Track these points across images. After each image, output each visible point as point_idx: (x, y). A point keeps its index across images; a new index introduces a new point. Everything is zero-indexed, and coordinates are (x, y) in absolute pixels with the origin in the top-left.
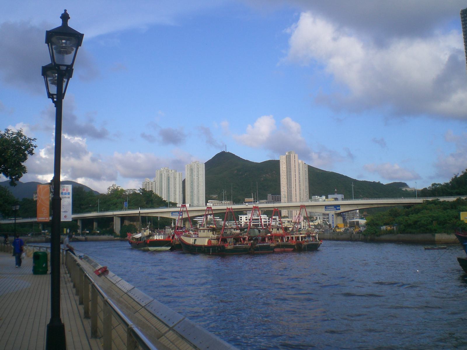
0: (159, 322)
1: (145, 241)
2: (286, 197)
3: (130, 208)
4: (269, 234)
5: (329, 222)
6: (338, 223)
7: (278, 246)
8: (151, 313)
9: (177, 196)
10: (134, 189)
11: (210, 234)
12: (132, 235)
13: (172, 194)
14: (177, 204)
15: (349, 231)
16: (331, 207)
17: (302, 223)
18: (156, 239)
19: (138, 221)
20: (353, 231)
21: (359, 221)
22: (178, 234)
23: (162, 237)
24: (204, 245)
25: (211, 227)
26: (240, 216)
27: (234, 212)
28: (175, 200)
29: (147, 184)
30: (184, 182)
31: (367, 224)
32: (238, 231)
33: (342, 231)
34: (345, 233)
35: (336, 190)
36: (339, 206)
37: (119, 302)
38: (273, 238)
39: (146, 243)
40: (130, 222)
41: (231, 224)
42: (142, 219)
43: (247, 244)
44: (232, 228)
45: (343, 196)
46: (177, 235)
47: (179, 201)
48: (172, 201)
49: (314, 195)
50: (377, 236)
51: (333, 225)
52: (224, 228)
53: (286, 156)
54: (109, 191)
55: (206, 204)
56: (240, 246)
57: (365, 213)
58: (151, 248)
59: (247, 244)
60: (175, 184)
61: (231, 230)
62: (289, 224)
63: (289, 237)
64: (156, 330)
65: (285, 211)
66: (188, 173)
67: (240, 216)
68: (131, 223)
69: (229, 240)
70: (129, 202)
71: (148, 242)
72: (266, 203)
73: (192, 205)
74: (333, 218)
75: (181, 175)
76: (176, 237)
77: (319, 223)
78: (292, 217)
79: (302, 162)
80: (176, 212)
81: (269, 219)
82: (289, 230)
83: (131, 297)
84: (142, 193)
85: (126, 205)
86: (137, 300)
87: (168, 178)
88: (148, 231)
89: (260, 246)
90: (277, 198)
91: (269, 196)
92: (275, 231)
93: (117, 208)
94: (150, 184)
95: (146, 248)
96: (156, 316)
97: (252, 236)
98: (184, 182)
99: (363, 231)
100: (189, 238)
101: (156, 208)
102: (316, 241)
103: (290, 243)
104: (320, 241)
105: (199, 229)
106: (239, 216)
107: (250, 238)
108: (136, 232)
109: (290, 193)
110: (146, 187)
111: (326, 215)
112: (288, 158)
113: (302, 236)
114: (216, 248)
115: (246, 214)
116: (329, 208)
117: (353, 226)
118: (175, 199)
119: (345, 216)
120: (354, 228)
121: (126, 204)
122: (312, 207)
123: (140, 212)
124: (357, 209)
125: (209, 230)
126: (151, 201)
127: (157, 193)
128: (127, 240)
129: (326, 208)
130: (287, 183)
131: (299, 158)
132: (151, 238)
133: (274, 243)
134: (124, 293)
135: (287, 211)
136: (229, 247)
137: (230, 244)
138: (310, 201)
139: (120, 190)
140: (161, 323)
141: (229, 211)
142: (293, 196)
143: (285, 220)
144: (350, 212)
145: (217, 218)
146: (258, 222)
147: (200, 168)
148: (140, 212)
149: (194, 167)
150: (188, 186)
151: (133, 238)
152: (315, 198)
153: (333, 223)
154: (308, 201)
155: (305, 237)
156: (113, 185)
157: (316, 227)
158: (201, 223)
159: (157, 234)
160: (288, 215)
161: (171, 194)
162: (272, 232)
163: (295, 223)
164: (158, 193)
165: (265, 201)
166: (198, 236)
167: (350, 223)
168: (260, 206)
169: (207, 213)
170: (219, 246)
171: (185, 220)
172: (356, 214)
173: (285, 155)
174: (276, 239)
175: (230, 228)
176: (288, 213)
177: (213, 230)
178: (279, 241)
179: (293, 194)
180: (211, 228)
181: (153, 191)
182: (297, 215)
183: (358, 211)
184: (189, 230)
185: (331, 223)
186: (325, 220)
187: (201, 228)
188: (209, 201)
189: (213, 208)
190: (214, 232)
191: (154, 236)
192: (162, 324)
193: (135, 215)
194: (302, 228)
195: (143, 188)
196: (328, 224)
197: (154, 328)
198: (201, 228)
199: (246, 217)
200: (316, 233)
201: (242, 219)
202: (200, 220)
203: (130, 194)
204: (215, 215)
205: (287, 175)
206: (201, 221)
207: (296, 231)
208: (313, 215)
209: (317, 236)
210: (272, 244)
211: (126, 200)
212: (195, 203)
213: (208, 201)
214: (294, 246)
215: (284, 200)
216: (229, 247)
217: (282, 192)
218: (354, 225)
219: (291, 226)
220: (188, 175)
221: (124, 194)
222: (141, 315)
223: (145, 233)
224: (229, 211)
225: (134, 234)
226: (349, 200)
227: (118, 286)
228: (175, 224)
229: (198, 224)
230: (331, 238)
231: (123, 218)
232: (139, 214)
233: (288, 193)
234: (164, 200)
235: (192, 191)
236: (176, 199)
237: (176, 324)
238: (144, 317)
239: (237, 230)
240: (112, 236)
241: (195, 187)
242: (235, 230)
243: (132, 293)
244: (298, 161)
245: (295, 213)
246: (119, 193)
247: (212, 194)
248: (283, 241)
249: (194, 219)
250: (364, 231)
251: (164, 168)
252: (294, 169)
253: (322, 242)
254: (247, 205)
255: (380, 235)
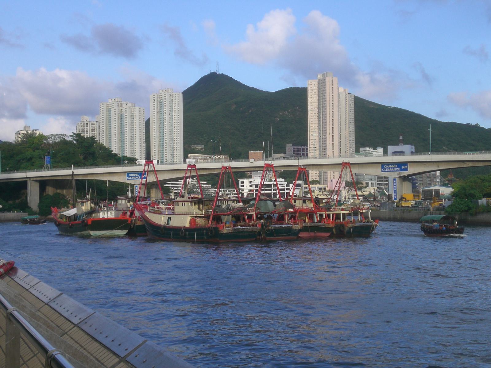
0: (103, 348)
1: (83, 221)
2: (317, 149)
3: (55, 167)
4: (291, 210)
5: (388, 191)
6: (404, 193)
7: (305, 229)
8: (88, 334)
9: (137, 147)
10: (63, 135)
11: (194, 209)
12: (59, 210)
13: (128, 143)
14: (136, 159)
15: (422, 206)
16: (392, 166)
17: (343, 192)
18: (103, 217)
19: (71, 187)
20: (430, 206)
21: (439, 190)
22: (140, 210)
23: (113, 214)
24: (184, 227)
25: (195, 198)
26: (240, 180)
27: (233, 172)
28: (132, 153)
29: (84, 126)
30: (148, 123)
31: (454, 195)
32: (240, 205)
33: (411, 206)
34: (415, 210)
35: (401, 138)
36: (405, 164)
37: (33, 317)
38: (297, 215)
39: (87, 225)
40: (57, 189)
41: (228, 193)
42: (77, 184)
43: (254, 225)
44: (230, 199)
45: (414, 147)
46: (138, 210)
47: (139, 155)
48: (129, 155)
49: (365, 146)
50: (471, 215)
51: (394, 196)
52: (217, 199)
53: (317, 80)
54: (18, 137)
55: (185, 161)
56: (243, 228)
57: (451, 177)
58: (92, 233)
59: (256, 225)
60: (133, 126)
61: (228, 202)
62: (321, 193)
63: (323, 214)
64: (96, 362)
65: (314, 172)
66: (154, 109)
67: (240, 180)
68: (59, 191)
69: (225, 219)
70: (54, 156)
71: (90, 223)
72: (284, 158)
73: (161, 162)
74: (395, 184)
75: (142, 112)
76: (137, 213)
77: (370, 193)
78: (325, 181)
79: (345, 91)
80: (134, 173)
81: (288, 185)
82: (323, 203)
83: (55, 310)
84: (77, 141)
85: (49, 161)
86: (66, 314)
87: (121, 117)
88: (89, 205)
89: (276, 229)
90: (302, 151)
91: (289, 147)
92: (301, 205)
93: (33, 165)
94: (91, 125)
95: (85, 233)
96: (97, 339)
97: (262, 212)
98: (148, 123)
99: (446, 207)
100: (159, 215)
101: (100, 166)
102: (368, 222)
103: (324, 224)
104: (374, 221)
105: (176, 200)
106: (239, 179)
107: (259, 216)
108: (67, 205)
109: (324, 143)
110: (83, 131)
111: (384, 180)
112: (322, 85)
113: (345, 213)
114: (205, 231)
115: (250, 177)
116: (388, 168)
117: (430, 198)
118: (133, 152)
119: (417, 182)
120: (432, 201)
121: (48, 160)
122: (360, 165)
123: (73, 172)
124: (438, 169)
125: (191, 202)
126: (93, 154)
127: (101, 142)
128: (51, 220)
129: (383, 167)
130: (319, 126)
131: (339, 85)
132: (94, 215)
133: (298, 224)
134: (44, 304)
135: (317, 172)
136: (226, 230)
137: (227, 225)
138: (356, 155)
139: (37, 135)
140: (105, 351)
141: (226, 171)
142: (328, 147)
143: (315, 188)
144: (424, 175)
145: (203, 184)
146: (271, 190)
147: (175, 100)
148: (73, 172)
149: (165, 99)
150: (155, 130)
151: (62, 217)
152: (366, 151)
153: (395, 192)
154: (354, 156)
155: (349, 214)
156: (25, 127)
157: (366, 198)
158: (176, 191)
159: (104, 209)
160: (320, 178)
161: (125, 142)
162: (295, 205)
163: (332, 192)
164: (103, 141)
165: (282, 155)
166: (174, 213)
167: (425, 192)
168: (276, 163)
169: (188, 175)
170: (209, 228)
171: (149, 186)
172: (435, 178)
173: (317, 79)
174: (302, 218)
175: (226, 200)
176: (320, 176)
177: (199, 202)
178: (307, 221)
179: (328, 144)
180: (195, 199)
181: (95, 138)
182: (334, 178)
183: (438, 173)
184: (159, 202)
185: (391, 192)
186: (382, 187)
187: (179, 199)
188: (189, 155)
189: (198, 166)
190: (201, 205)
191: (99, 213)
192: (108, 353)
193: (64, 178)
194: (343, 200)
195: (78, 133)
196: (387, 194)
197: (94, 359)
198: (179, 199)
199: (250, 182)
200: (368, 208)
201: (244, 184)
202: (176, 187)
203: (56, 143)
204: (200, 178)
205: (319, 112)
206: (176, 188)
207: (335, 204)
208: (362, 180)
209: (370, 213)
210: (295, 225)
211: (49, 153)
212: (167, 158)
213: (188, 155)
214: (332, 228)
215: (312, 154)
216: (225, 231)
217: (311, 141)
218: (431, 196)
219: (325, 197)
220: (154, 111)
221: (45, 142)
222: (72, 338)
223: (83, 207)
224: (226, 171)
225: (63, 209)
226: (424, 155)
227: (33, 293)
228: (132, 192)
229: (172, 192)
230: (392, 216)
231: (43, 183)
232: (71, 177)
233: (320, 142)
234: (115, 153)
235: (161, 138)
236: (135, 152)
237: (131, 352)
238: (76, 342)
239: (239, 202)
240: (25, 213)
241: (166, 131)
242: (235, 202)
243: (57, 304)
244: (338, 89)
245: (333, 176)
246: (36, 141)
247: (195, 144)
248: (313, 221)
249: (165, 185)
250: (449, 206)
251: (113, 100)
252: (331, 103)
253: (377, 223)
254: (253, 163)
255: (476, 214)
